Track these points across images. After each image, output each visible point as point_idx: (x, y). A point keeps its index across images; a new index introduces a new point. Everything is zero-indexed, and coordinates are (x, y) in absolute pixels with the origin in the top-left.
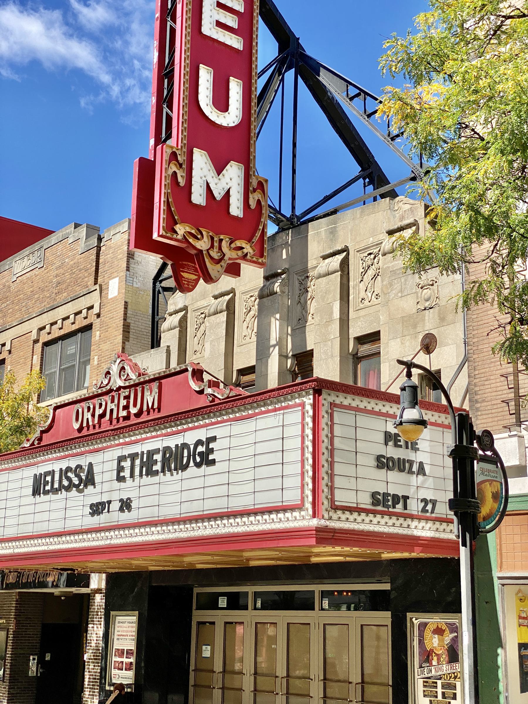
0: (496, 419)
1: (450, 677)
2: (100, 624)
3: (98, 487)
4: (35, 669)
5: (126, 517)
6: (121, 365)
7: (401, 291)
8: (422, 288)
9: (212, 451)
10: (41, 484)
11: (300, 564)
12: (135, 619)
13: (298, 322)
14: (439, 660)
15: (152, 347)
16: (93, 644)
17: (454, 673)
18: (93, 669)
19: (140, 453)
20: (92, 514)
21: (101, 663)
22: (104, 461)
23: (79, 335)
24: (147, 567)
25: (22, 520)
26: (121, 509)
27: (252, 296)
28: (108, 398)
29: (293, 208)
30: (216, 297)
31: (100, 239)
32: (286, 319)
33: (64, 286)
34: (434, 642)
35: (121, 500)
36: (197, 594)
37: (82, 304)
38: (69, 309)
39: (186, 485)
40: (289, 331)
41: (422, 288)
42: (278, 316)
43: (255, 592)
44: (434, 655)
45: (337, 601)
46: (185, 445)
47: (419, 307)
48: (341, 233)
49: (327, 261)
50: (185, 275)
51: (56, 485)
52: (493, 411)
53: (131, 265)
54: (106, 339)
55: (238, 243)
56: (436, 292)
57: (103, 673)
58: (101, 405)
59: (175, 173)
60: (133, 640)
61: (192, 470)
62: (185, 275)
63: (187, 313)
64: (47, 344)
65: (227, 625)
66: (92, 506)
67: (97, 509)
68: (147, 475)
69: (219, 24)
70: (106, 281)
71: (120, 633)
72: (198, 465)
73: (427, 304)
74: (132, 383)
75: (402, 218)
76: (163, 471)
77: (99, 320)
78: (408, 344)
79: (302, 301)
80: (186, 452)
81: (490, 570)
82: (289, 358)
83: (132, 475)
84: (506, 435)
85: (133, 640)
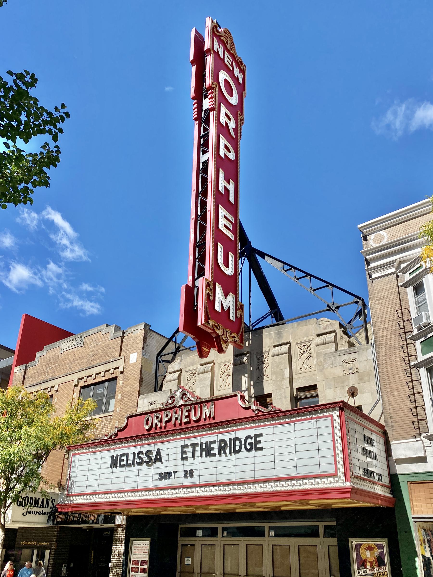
0: (406, 432)
1: (380, 575)
2: (121, 546)
3: (165, 464)
4: (65, 572)
5: (189, 481)
6: (183, 393)
7: (332, 364)
8: (346, 363)
9: (259, 442)
10: (117, 461)
11: (270, 511)
12: (148, 542)
13: (258, 378)
14: (371, 566)
15: (155, 391)
16: (116, 557)
17: (382, 572)
18: (116, 572)
19: (199, 443)
20: (161, 479)
21: (122, 569)
22: (170, 449)
23: (107, 383)
24: (235, 509)
25: (101, 482)
26: (185, 476)
27: (225, 365)
28: (172, 411)
29: (250, 322)
30: (202, 365)
31: (124, 333)
32: (251, 378)
33: (97, 357)
34: (367, 555)
35: (186, 471)
36: (181, 528)
37: (112, 366)
38: (102, 368)
39: (238, 462)
40: (252, 384)
41: (346, 363)
42: (246, 375)
43: (223, 527)
44: (367, 562)
45: (281, 533)
46: (236, 439)
47: (345, 372)
48: (284, 334)
49: (277, 348)
50: (204, 348)
51: (130, 462)
52: (404, 427)
53: (145, 347)
54: (128, 384)
55: (233, 334)
56: (356, 365)
57: (124, 575)
58: (167, 416)
59: (208, 293)
60: (146, 555)
61: (244, 453)
62: (204, 348)
63: (181, 372)
64: (82, 387)
65: (203, 546)
66: (160, 474)
67: (163, 476)
68: (206, 456)
69: (225, 226)
70: (128, 354)
71: (135, 551)
72: (249, 450)
73: (351, 371)
74: (191, 402)
75: (325, 328)
76: (220, 454)
77: (122, 375)
78: (338, 391)
79: (260, 368)
80: (238, 443)
81: (406, 514)
82: (253, 398)
83: (194, 456)
84: (414, 440)
85: (146, 555)
